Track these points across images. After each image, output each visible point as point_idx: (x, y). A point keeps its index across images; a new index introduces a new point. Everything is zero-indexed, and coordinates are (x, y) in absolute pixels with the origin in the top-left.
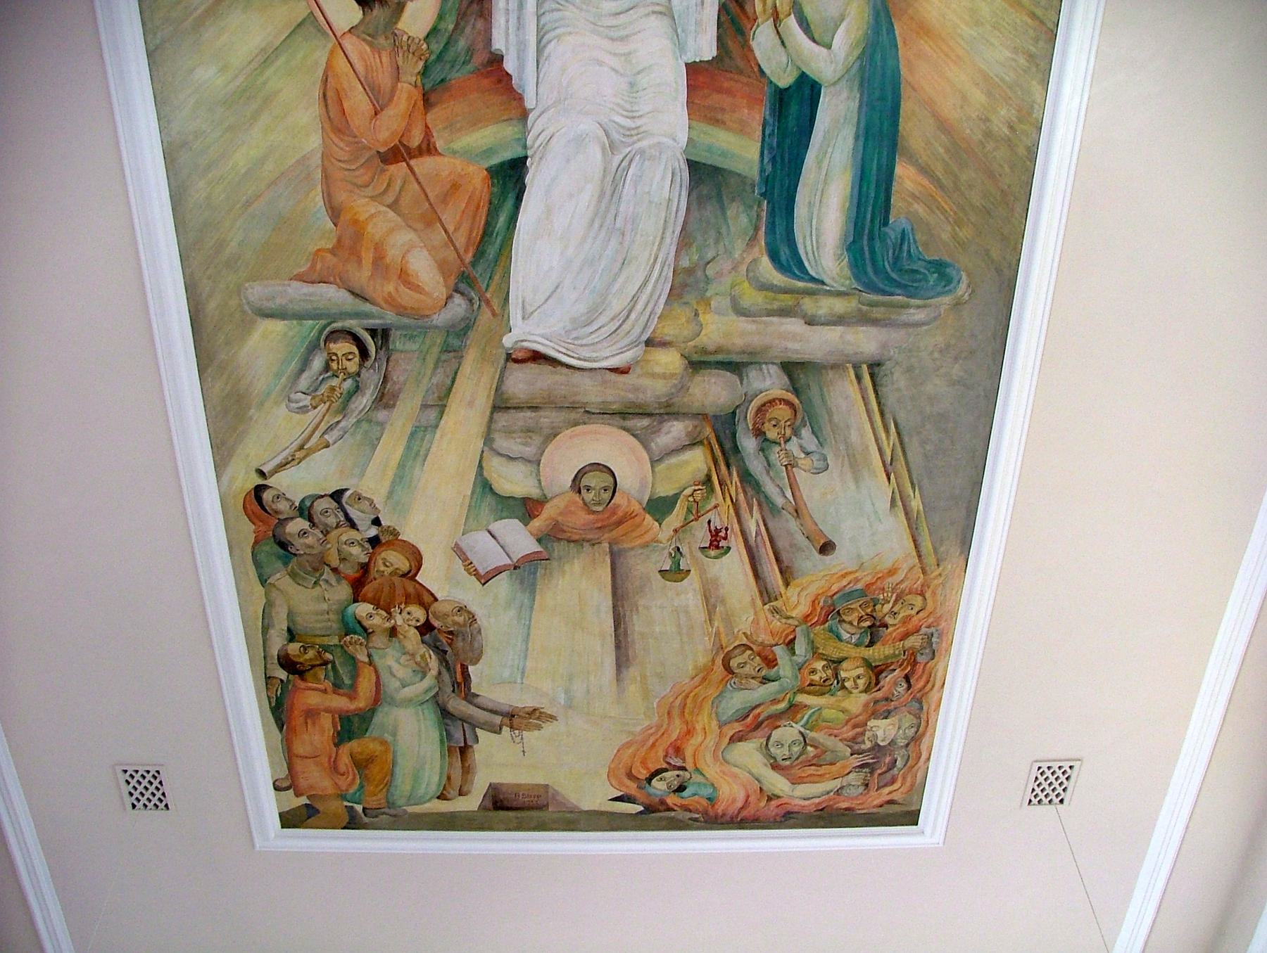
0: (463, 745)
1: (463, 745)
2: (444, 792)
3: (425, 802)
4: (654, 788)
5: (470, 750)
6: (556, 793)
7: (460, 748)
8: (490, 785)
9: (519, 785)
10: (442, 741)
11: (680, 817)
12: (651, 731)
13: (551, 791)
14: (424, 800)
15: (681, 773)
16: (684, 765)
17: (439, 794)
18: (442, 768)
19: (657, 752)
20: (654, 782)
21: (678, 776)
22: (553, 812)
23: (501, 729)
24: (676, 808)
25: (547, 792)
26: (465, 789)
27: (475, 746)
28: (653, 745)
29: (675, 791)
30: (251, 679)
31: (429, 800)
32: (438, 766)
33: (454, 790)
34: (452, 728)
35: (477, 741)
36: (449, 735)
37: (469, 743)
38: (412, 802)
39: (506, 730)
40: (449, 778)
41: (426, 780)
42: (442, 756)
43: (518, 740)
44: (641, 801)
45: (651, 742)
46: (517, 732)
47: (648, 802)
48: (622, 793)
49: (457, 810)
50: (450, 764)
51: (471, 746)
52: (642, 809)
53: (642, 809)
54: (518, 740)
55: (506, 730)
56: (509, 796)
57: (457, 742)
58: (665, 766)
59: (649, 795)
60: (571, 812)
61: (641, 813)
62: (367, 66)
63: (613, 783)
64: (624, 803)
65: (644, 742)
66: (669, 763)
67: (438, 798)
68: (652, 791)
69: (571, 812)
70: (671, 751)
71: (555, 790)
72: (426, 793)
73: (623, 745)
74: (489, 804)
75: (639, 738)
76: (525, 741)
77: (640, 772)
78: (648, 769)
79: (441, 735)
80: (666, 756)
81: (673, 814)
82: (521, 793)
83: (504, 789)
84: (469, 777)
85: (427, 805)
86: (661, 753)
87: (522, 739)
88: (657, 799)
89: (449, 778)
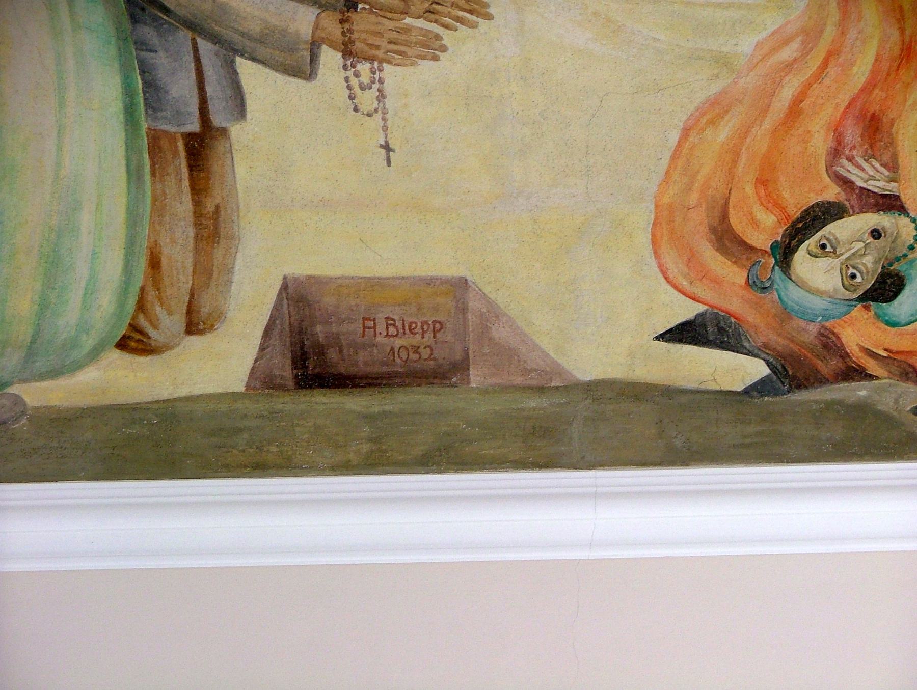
0: (194, 126)
1: (194, 126)
2: (142, 322)
3: (77, 366)
4: (801, 285)
5: (220, 146)
6: (493, 313)
7: (189, 137)
8: (285, 287)
9: (375, 284)
10: (129, 111)
11: (886, 403)
12: (788, 53)
13: (474, 304)
14: (77, 354)
15: (884, 220)
16: (892, 188)
17: (123, 331)
18: (133, 220)
19: (806, 139)
20: (801, 259)
21: (876, 234)
22: (484, 392)
23: (314, 58)
24: (872, 367)
25: (464, 310)
26: (205, 308)
27: (235, 130)
28: (794, 111)
29: (865, 298)
30: (695, 347)
31: (94, 355)
32: (120, 215)
33: (170, 313)
34: (161, 61)
35: (239, 107)
36: (152, 86)
37: (217, 120)
38: (40, 365)
39: (330, 58)
40: (155, 263)
41: (82, 270)
42: (134, 174)
43: (367, 99)
44: (761, 340)
45: (787, 93)
46: (364, 68)
47: (779, 342)
48: (701, 308)
49: (183, 392)
50: (159, 207)
51: (224, 132)
52: (764, 370)
53: (764, 370)
54: (367, 99)
55: (330, 58)
56: (345, 328)
57: (178, 114)
58: (832, 193)
59: (785, 314)
60: (541, 390)
61: (760, 388)
62: (382, 378)
63: (673, 272)
64: (706, 351)
65: (768, 94)
66: (846, 183)
67: (123, 345)
68: (794, 294)
69: (541, 390)
70: (852, 134)
71: (490, 303)
72: (84, 327)
73: (701, 111)
74: (285, 370)
75: (749, 82)
76: (389, 103)
77: (755, 223)
78: (783, 209)
79: (128, 92)
80: (836, 153)
81: (860, 391)
82: (380, 317)
83: (328, 301)
84: (219, 253)
85: (89, 376)
86: (820, 143)
87: (381, 96)
88: (813, 329)
89: (155, 263)
